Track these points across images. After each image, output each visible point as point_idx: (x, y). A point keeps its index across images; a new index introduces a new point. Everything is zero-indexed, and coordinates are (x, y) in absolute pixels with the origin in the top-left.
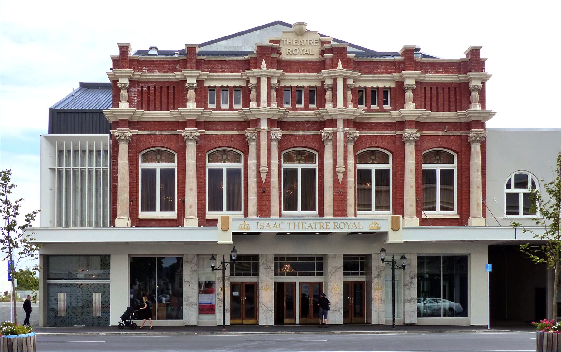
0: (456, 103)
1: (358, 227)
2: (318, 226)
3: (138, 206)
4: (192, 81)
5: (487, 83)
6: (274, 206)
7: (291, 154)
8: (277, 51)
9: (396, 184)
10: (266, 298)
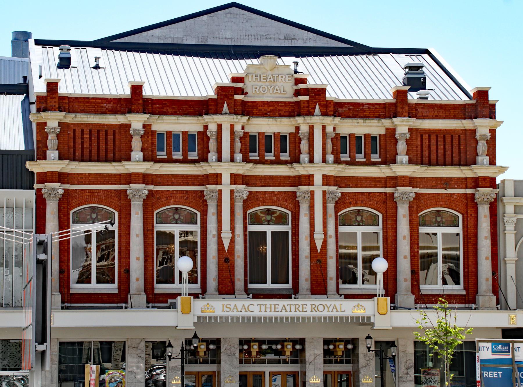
1: (339, 309)
2: (293, 308)
7: (259, 213)
9: (387, 252)
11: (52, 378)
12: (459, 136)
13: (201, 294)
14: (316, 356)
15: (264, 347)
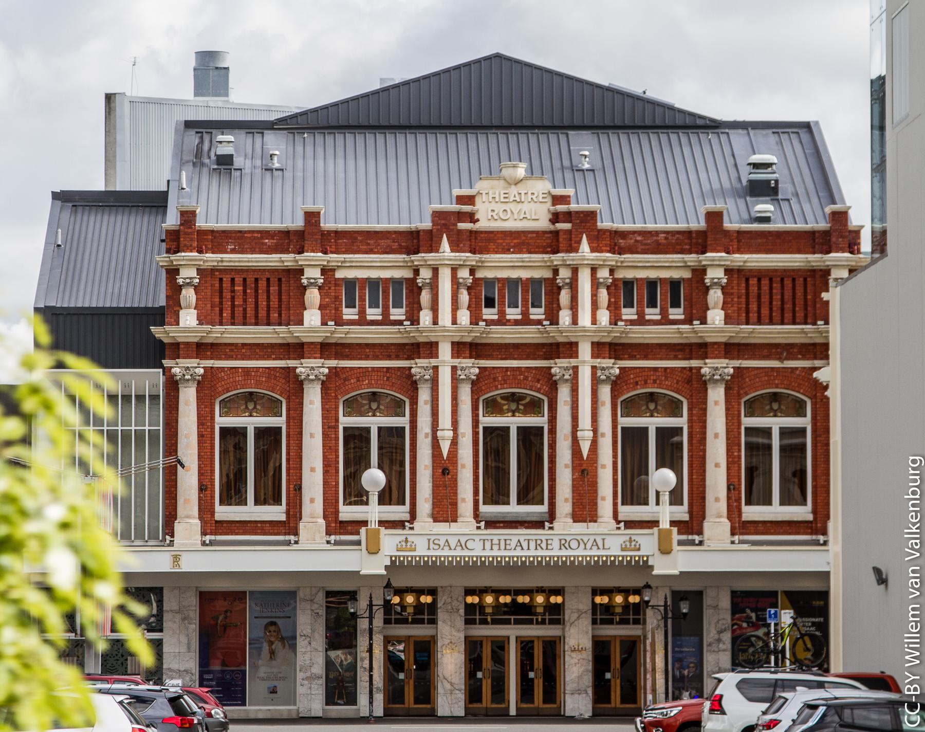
2: (532, 545)
3: (213, 497)
4: (313, 274)
6: (464, 500)
7: (499, 400)
8: (471, 217)
10: (450, 664)
11: (189, 643)
13: (408, 521)
14: (581, 613)
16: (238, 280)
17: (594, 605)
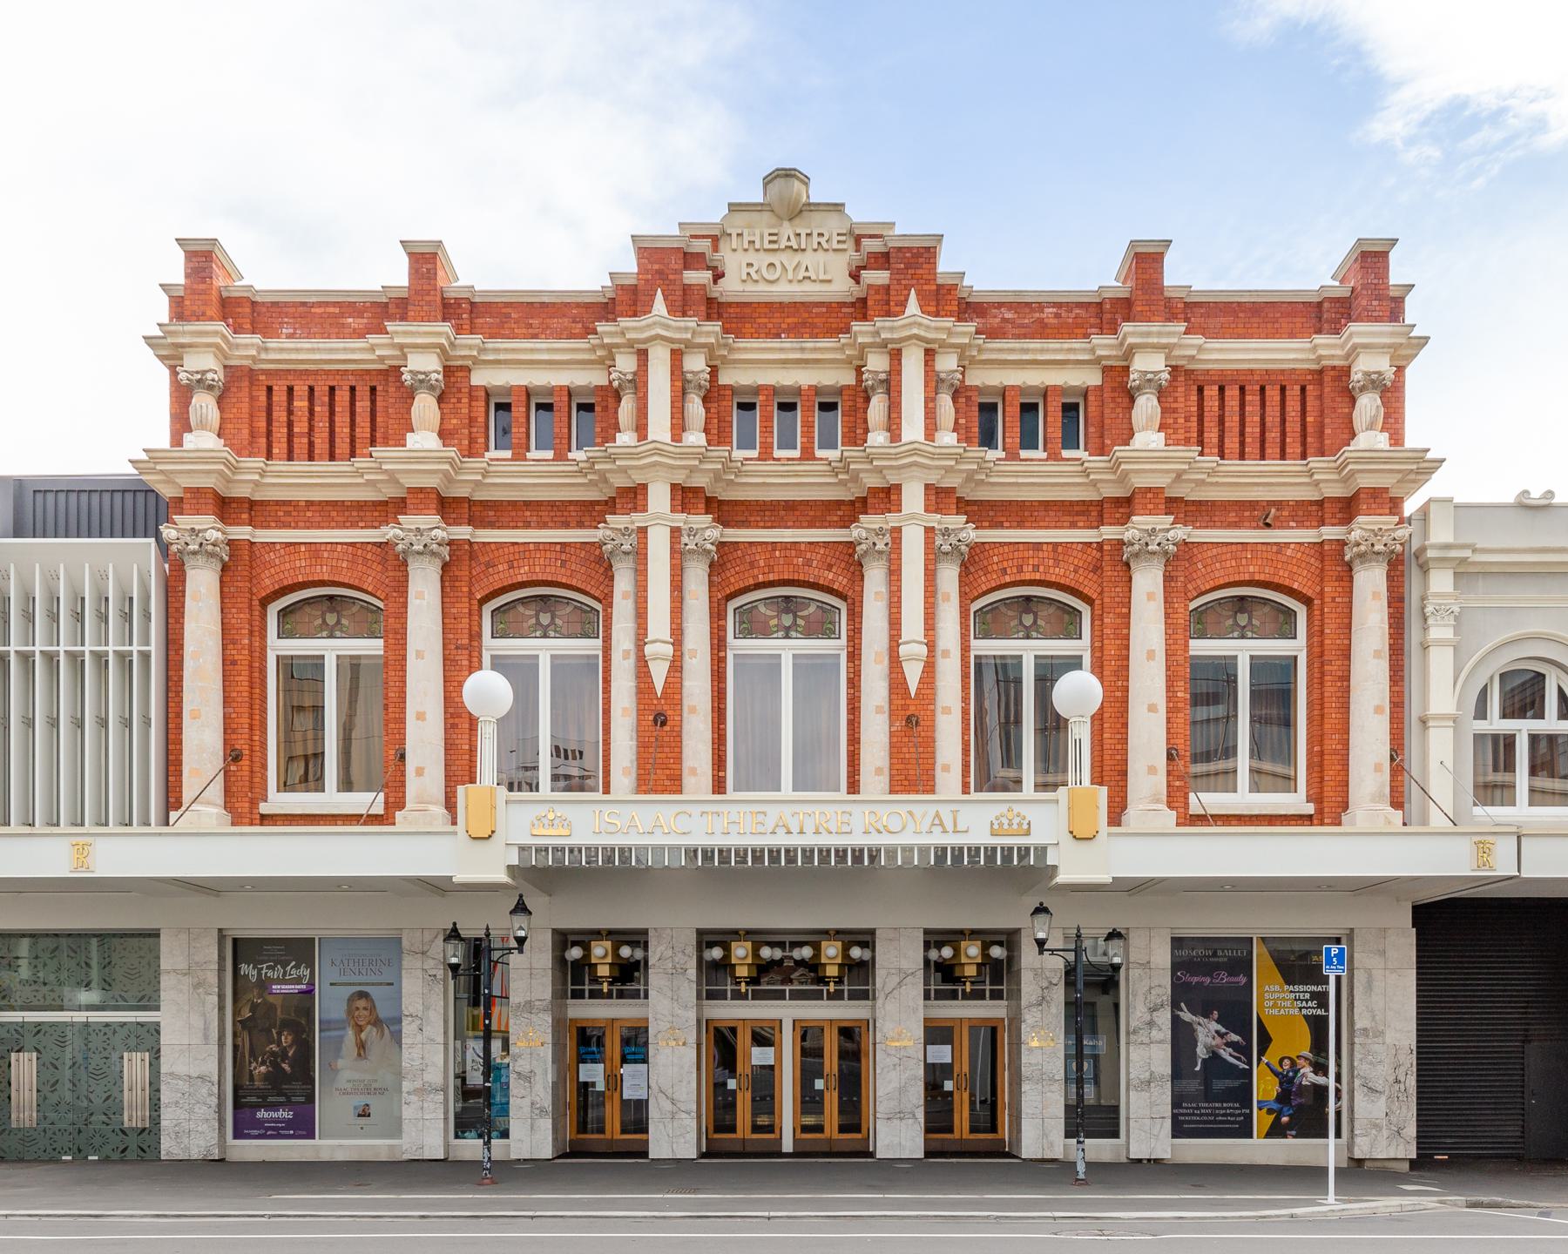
0: (1304, 436)
1: (949, 827)
5: (1408, 371)
6: (693, 771)
11: (206, 1029)
12: (1303, 389)
14: (904, 975)
15: (766, 952)
16: (301, 390)
17: (927, 962)
